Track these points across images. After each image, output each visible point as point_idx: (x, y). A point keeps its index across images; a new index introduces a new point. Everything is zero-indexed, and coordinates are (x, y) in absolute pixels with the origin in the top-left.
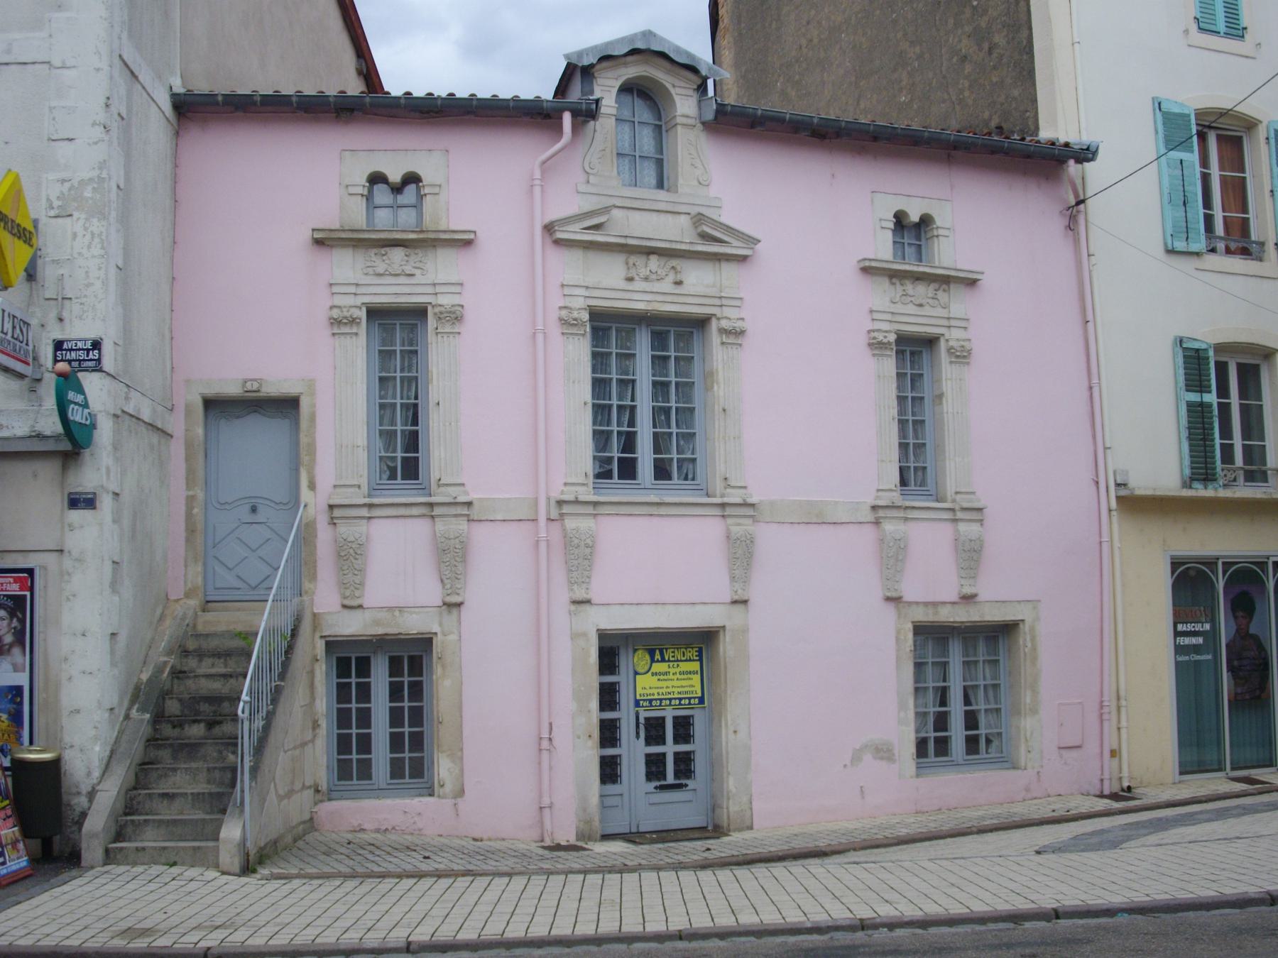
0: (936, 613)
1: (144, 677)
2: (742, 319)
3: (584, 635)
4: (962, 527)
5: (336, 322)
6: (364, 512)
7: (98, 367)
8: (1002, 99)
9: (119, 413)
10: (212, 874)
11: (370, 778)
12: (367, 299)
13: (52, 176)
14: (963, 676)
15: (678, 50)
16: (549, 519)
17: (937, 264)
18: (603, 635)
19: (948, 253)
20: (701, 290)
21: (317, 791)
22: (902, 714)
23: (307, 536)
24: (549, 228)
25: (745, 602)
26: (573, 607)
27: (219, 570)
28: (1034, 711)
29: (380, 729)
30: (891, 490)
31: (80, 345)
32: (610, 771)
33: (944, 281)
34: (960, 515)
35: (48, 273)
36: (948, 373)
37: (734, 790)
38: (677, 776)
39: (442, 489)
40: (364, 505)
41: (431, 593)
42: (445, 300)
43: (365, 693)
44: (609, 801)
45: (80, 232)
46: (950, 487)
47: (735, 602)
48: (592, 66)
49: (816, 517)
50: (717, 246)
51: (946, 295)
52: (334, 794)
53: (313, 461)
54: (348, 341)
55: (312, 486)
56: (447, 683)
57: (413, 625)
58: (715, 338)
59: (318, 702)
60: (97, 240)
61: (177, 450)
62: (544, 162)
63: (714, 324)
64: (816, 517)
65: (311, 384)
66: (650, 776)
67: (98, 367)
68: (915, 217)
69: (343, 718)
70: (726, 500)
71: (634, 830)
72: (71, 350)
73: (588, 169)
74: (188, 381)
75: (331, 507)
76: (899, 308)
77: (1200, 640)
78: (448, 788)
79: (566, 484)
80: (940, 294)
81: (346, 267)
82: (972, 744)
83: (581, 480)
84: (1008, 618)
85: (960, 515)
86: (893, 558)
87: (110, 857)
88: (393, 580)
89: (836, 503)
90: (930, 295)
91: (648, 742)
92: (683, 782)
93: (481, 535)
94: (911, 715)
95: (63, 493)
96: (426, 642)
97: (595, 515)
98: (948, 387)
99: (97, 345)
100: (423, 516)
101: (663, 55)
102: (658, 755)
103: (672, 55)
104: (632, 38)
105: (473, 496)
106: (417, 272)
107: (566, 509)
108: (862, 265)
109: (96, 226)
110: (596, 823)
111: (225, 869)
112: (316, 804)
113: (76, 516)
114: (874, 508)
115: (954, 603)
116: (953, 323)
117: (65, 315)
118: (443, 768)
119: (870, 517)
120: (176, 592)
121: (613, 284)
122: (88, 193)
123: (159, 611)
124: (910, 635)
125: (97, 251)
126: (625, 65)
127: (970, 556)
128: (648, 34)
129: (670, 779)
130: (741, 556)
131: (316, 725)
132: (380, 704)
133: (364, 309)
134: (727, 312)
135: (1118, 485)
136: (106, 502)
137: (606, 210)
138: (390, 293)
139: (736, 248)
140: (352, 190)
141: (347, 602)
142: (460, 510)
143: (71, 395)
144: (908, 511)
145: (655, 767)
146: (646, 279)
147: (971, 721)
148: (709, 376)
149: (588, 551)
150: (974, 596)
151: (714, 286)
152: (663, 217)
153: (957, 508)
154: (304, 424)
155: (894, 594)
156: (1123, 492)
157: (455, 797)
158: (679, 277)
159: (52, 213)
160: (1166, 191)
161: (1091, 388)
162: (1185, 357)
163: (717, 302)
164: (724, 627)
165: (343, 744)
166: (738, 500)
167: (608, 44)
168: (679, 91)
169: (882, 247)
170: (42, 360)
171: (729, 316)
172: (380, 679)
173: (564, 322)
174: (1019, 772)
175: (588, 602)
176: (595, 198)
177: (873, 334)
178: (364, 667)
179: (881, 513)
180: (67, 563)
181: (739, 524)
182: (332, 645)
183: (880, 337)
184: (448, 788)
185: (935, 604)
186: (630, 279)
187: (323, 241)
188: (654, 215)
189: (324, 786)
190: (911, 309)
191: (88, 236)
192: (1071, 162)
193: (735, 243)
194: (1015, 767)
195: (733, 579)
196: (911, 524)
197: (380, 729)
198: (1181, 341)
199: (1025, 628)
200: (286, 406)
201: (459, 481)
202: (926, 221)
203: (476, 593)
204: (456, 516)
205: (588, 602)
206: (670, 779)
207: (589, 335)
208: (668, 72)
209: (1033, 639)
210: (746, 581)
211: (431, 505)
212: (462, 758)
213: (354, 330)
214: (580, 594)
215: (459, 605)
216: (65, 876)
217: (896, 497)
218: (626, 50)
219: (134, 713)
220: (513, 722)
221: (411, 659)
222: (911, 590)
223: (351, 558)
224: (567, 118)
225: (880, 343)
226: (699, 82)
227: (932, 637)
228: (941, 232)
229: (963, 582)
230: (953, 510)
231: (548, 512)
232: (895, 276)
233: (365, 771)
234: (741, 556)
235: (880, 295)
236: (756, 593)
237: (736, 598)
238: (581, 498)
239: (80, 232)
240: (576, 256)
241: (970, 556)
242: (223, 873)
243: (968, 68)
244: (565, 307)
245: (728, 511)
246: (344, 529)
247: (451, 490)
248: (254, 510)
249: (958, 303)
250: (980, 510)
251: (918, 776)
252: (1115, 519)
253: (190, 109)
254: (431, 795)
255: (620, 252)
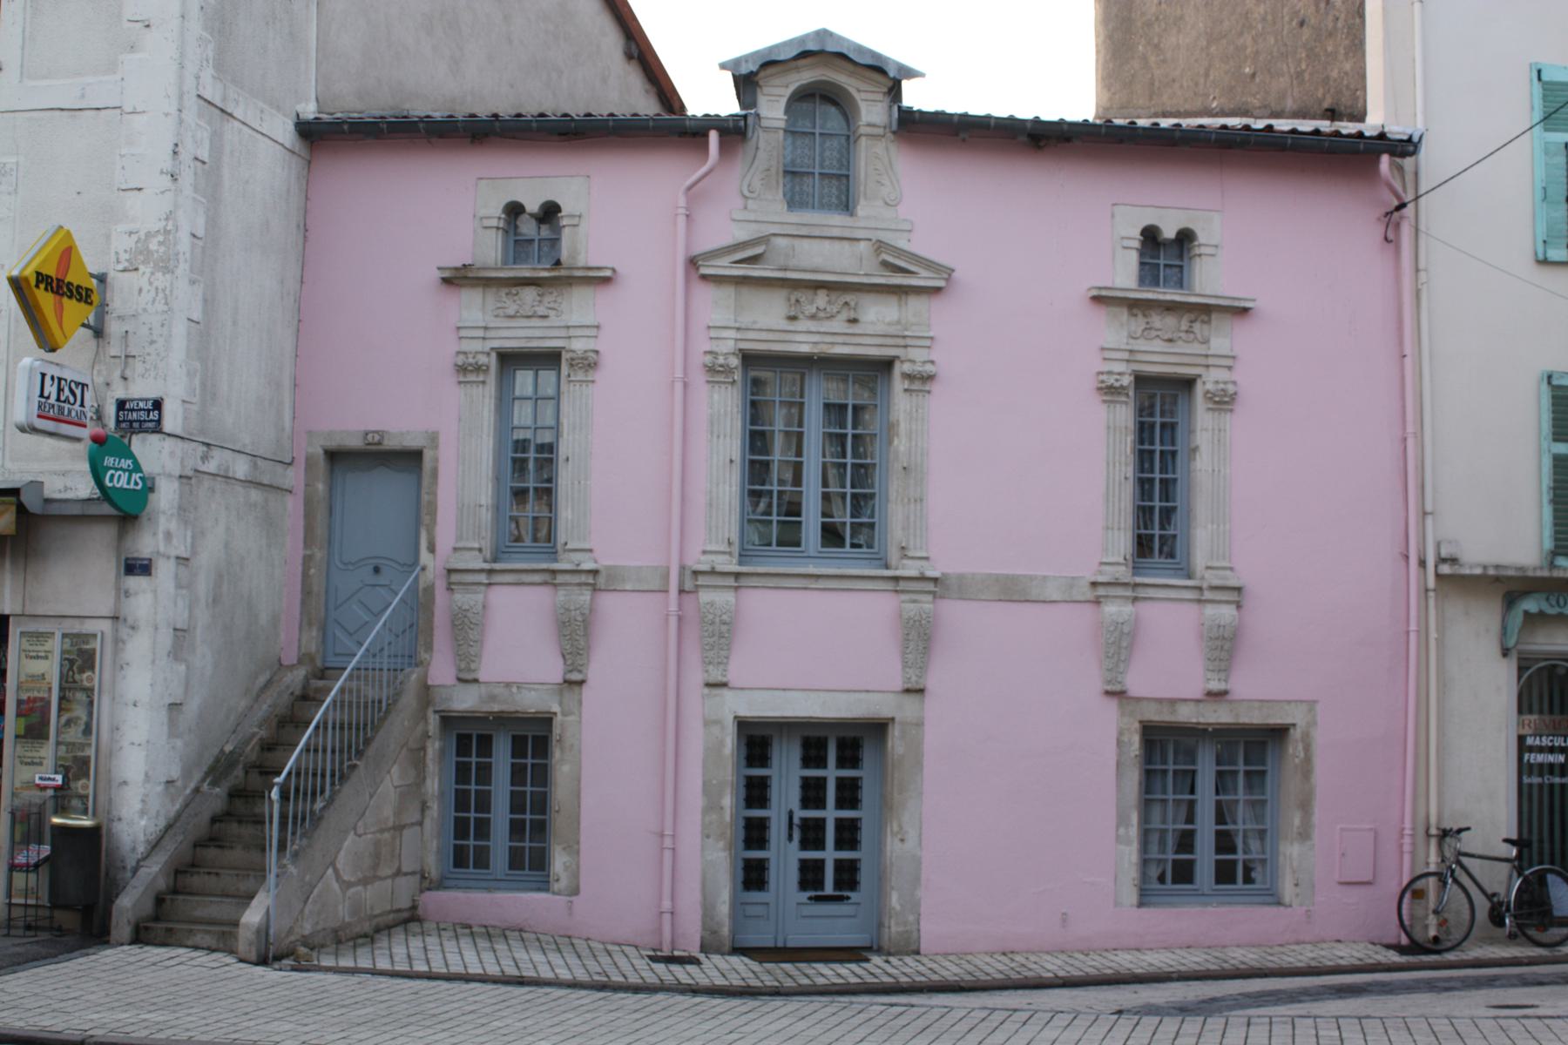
0: (1174, 712)
1: (228, 748)
2: (932, 362)
3: (717, 722)
4: (1210, 610)
5: (462, 369)
6: (483, 578)
7: (157, 428)
8: (1335, 74)
9: (190, 473)
10: (230, 959)
11: (487, 867)
12: (497, 344)
13: (121, 228)
14: (1207, 790)
15: (861, 49)
16: (681, 591)
17: (1198, 291)
18: (743, 725)
19: (1210, 278)
20: (880, 329)
21: (423, 877)
22: (1122, 831)
23: (421, 602)
24: (693, 262)
25: (921, 691)
26: (706, 691)
27: (339, 633)
28: (1305, 835)
29: (500, 815)
30: (1118, 564)
31: (142, 405)
32: (754, 876)
33: (1205, 311)
34: (1208, 595)
35: (114, 328)
36: (1203, 424)
37: (898, 908)
38: (838, 884)
39: (566, 555)
40: (481, 571)
41: (551, 669)
42: (579, 345)
43: (485, 773)
44: (751, 910)
45: (146, 287)
46: (1200, 559)
47: (908, 691)
48: (752, 74)
49: (1012, 591)
50: (905, 280)
51: (1205, 327)
52: (448, 883)
53: (434, 521)
54: (477, 391)
55: (432, 549)
56: (566, 768)
57: (530, 702)
58: (898, 385)
59: (429, 782)
60: (161, 295)
61: (293, 507)
62: (689, 188)
63: (898, 368)
64: (1012, 591)
65: (434, 438)
66: (804, 885)
67: (157, 428)
68: (1169, 232)
69: (461, 801)
70: (898, 573)
71: (780, 944)
72: (132, 410)
73: (746, 193)
74: (309, 433)
75: (450, 571)
76: (1141, 345)
77: (1561, 758)
78: (563, 883)
79: (704, 552)
80: (1197, 326)
81: (473, 308)
82: (1225, 874)
83: (724, 547)
84: (1271, 721)
85: (1208, 595)
86: (1119, 646)
87: (141, 936)
88: (513, 650)
89: (1045, 578)
90: (1184, 328)
91: (804, 845)
92: (845, 894)
93: (609, 603)
94: (1134, 832)
95: (118, 558)
96: (546, 721)
97: (737, 588)
98: (1202, 439)
99: (158, 405)
100: (545, 583)
101: (842, 56)
102: (816, 861)
103: (851, 56)
104: (802, 40)
105: (604, 561)
106: (552, 313)
107: (701, 581)
108: (1095, 293)
109: (161, 280)
110: (725, 931)
111: (242, 956)
112: (422, 891)
113: (134, 582)
114: (1094, 584)
115: (1198, 701)
116: (1211, 361)
117: (128, 373)
118: (559, 862)
119: (1090, 594)
120: (290, 657)
121: (769, 322)
122: (153, 246)
123: (262, 680)
124: (1136, 739)
125: (160, 307)
126: (797, 69)
127: (1224, 648)
128: (823, 34)
129: (829, 888)
130: (919, 640)
131: (424, 807)
132: (501, 788)
133: (494, 355)
134: (914, 354)
135: (1442, 560)
136: (165, 571)
137: (764, 240)
138: (518, 336)
139: (923, 279)
140: (487, 223)
141: (463, 676)
142: (583, 578)
143: (109, 461)
144: (1140, 589)
145: (810, 875)
146: (813, 317)
147: (1225, 842)
148: (891, 429)
149: (724, 628)
150: (1224, 693)
151: (898, 322)
152: (837, 245)
153: (1205, 585)
154: (426, 481)
155: (1117, 688)
156: (1445, 569)
157: (570, 895)
158: (852, 315)
159: (120, 267)
160: (1539, 186)
161: (1405, 439)
162: (1554, 397)
163: (901, 342)
164: (893, 719)
165: (461, 828)
166: (913, 573)
167: (771, 49)
168: (863, 95)
169: (1124, 274)
170: (106, 421)
171: (913, 359)
172: (502, 759)
173: (711, 370)
174: (1282, 908)
175: (724, 685)
176: (754, 226)
177: (1102, 377)
178: (485, 744)
179: (1101, 591)
180: (124, 632)
181: (914, 601)
182: (448, 721)
183: (1111, 380)
184: (563, 883)
185: (1173, 702)
186: (793, 318)
187: (457, 279)
188: (827, 243)
189: (434, 873)
190: (1158, 345)
191: (153, 293)
192: (1385, 159)
193: (924, 273)
194: (1279, 903)
195: (905, 665)
196: (1141, 605)
197: (500, 815)
198: (1550, 377)
199: (1296, 734)
200: (410, 460)
201: (587, 546)
202: (1185, 238)
203: (597, 671)
204: (579, 585)
205: (724, 685)
206: (829, 888)
207: (739, 384)
208: (851, 74)
209: (1307, 748)
210: (923, 668)
211: (554, 572)
212: (578, 852)
213: (481, 378)
214: (716, 676)
215: (581, 683)
216: (91, 951)
217: (1123, 573)
218: (795, 53)
219: (205, 787)
220: (644, 812)
221: (534, 739)
222: (1137, 682)
223: (466, 629)
224: (713, 136)
225: (1111, 387)
226: (890, 84)
227: (1165, 749)
228: (1203, 250)
229: (1209, 675)
230: (1200, 589)
231: (681, 582)
232: (1135, 306)
233: (482, 860)
234: (919, 640)
235: (1114, 331)
236: (934, 681)
237: (909, 686)
238: (719, 568)
239: (146, 287)
240: (728, 292)
241: (1224, 648)
242: (241, 961)
243: (1306, 33)
244: (710, 352)
245: (902, 585)
246: (462, 598)
247: (577, 557)
248: (377, 570)
249: (1221, 339)
250: (1239, 589)
251: (1141, 905)
252: (1432, 602)
253: (317, 136)
254: (547, 890)
255: (782, 287)
